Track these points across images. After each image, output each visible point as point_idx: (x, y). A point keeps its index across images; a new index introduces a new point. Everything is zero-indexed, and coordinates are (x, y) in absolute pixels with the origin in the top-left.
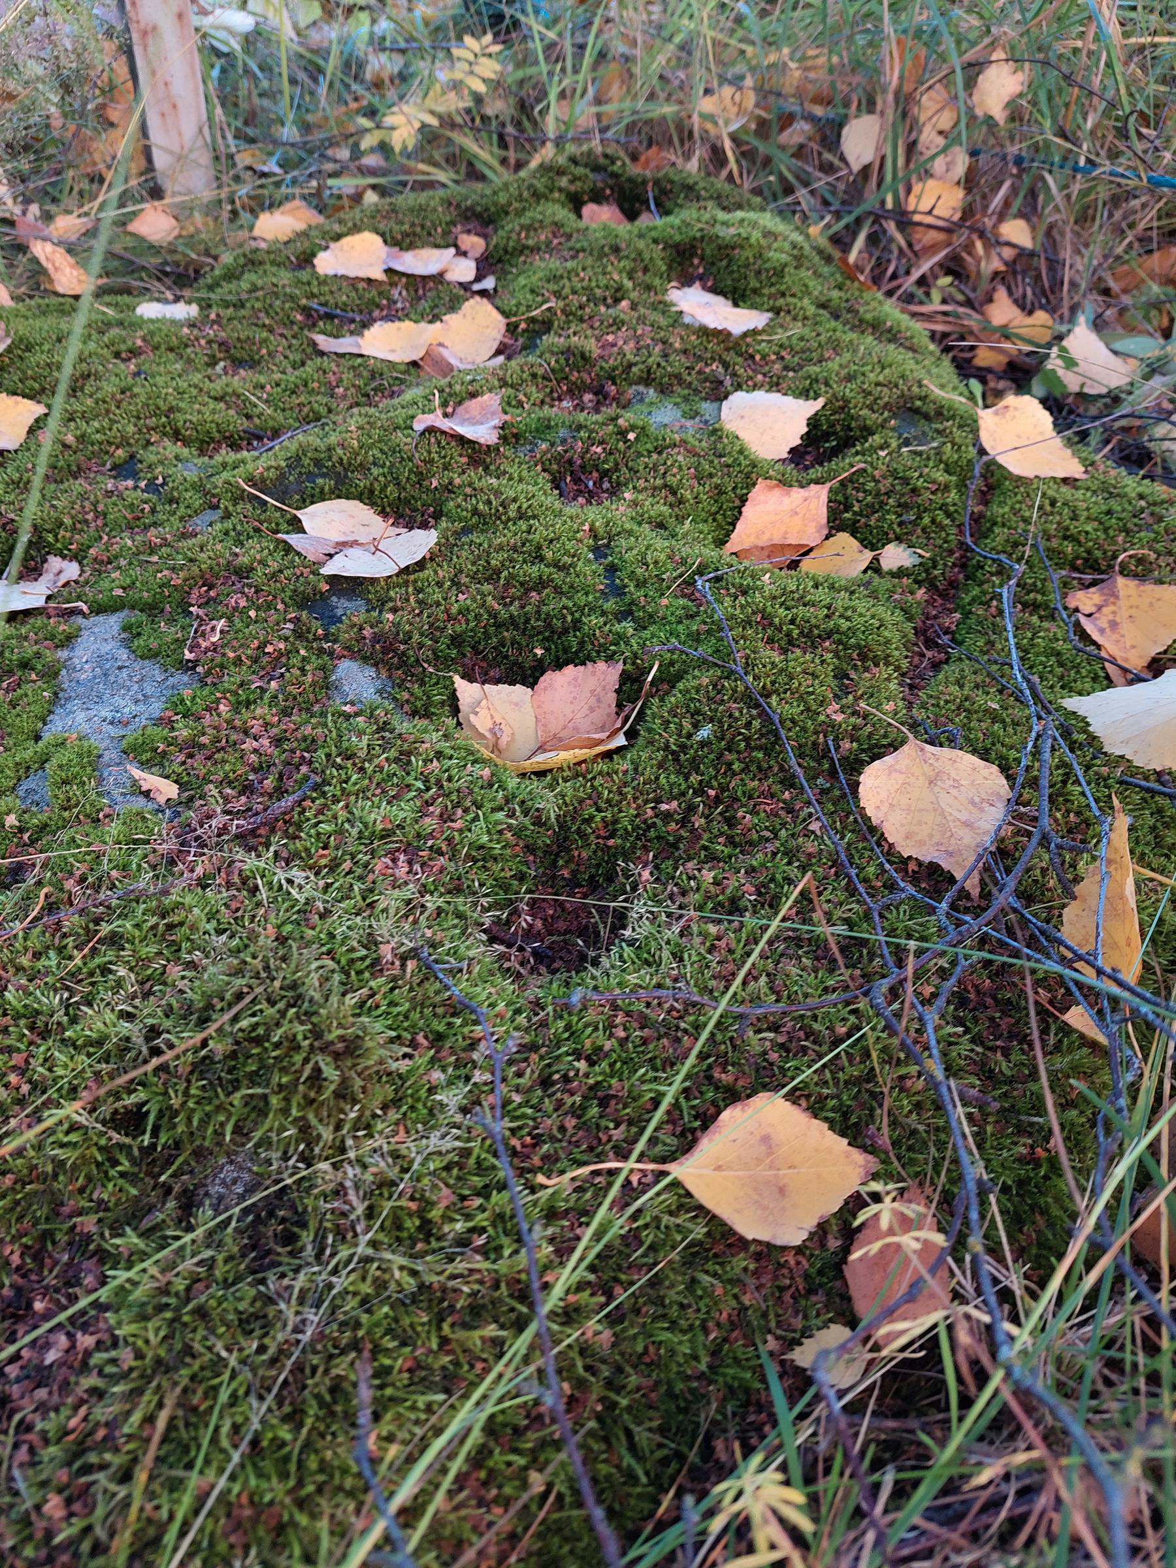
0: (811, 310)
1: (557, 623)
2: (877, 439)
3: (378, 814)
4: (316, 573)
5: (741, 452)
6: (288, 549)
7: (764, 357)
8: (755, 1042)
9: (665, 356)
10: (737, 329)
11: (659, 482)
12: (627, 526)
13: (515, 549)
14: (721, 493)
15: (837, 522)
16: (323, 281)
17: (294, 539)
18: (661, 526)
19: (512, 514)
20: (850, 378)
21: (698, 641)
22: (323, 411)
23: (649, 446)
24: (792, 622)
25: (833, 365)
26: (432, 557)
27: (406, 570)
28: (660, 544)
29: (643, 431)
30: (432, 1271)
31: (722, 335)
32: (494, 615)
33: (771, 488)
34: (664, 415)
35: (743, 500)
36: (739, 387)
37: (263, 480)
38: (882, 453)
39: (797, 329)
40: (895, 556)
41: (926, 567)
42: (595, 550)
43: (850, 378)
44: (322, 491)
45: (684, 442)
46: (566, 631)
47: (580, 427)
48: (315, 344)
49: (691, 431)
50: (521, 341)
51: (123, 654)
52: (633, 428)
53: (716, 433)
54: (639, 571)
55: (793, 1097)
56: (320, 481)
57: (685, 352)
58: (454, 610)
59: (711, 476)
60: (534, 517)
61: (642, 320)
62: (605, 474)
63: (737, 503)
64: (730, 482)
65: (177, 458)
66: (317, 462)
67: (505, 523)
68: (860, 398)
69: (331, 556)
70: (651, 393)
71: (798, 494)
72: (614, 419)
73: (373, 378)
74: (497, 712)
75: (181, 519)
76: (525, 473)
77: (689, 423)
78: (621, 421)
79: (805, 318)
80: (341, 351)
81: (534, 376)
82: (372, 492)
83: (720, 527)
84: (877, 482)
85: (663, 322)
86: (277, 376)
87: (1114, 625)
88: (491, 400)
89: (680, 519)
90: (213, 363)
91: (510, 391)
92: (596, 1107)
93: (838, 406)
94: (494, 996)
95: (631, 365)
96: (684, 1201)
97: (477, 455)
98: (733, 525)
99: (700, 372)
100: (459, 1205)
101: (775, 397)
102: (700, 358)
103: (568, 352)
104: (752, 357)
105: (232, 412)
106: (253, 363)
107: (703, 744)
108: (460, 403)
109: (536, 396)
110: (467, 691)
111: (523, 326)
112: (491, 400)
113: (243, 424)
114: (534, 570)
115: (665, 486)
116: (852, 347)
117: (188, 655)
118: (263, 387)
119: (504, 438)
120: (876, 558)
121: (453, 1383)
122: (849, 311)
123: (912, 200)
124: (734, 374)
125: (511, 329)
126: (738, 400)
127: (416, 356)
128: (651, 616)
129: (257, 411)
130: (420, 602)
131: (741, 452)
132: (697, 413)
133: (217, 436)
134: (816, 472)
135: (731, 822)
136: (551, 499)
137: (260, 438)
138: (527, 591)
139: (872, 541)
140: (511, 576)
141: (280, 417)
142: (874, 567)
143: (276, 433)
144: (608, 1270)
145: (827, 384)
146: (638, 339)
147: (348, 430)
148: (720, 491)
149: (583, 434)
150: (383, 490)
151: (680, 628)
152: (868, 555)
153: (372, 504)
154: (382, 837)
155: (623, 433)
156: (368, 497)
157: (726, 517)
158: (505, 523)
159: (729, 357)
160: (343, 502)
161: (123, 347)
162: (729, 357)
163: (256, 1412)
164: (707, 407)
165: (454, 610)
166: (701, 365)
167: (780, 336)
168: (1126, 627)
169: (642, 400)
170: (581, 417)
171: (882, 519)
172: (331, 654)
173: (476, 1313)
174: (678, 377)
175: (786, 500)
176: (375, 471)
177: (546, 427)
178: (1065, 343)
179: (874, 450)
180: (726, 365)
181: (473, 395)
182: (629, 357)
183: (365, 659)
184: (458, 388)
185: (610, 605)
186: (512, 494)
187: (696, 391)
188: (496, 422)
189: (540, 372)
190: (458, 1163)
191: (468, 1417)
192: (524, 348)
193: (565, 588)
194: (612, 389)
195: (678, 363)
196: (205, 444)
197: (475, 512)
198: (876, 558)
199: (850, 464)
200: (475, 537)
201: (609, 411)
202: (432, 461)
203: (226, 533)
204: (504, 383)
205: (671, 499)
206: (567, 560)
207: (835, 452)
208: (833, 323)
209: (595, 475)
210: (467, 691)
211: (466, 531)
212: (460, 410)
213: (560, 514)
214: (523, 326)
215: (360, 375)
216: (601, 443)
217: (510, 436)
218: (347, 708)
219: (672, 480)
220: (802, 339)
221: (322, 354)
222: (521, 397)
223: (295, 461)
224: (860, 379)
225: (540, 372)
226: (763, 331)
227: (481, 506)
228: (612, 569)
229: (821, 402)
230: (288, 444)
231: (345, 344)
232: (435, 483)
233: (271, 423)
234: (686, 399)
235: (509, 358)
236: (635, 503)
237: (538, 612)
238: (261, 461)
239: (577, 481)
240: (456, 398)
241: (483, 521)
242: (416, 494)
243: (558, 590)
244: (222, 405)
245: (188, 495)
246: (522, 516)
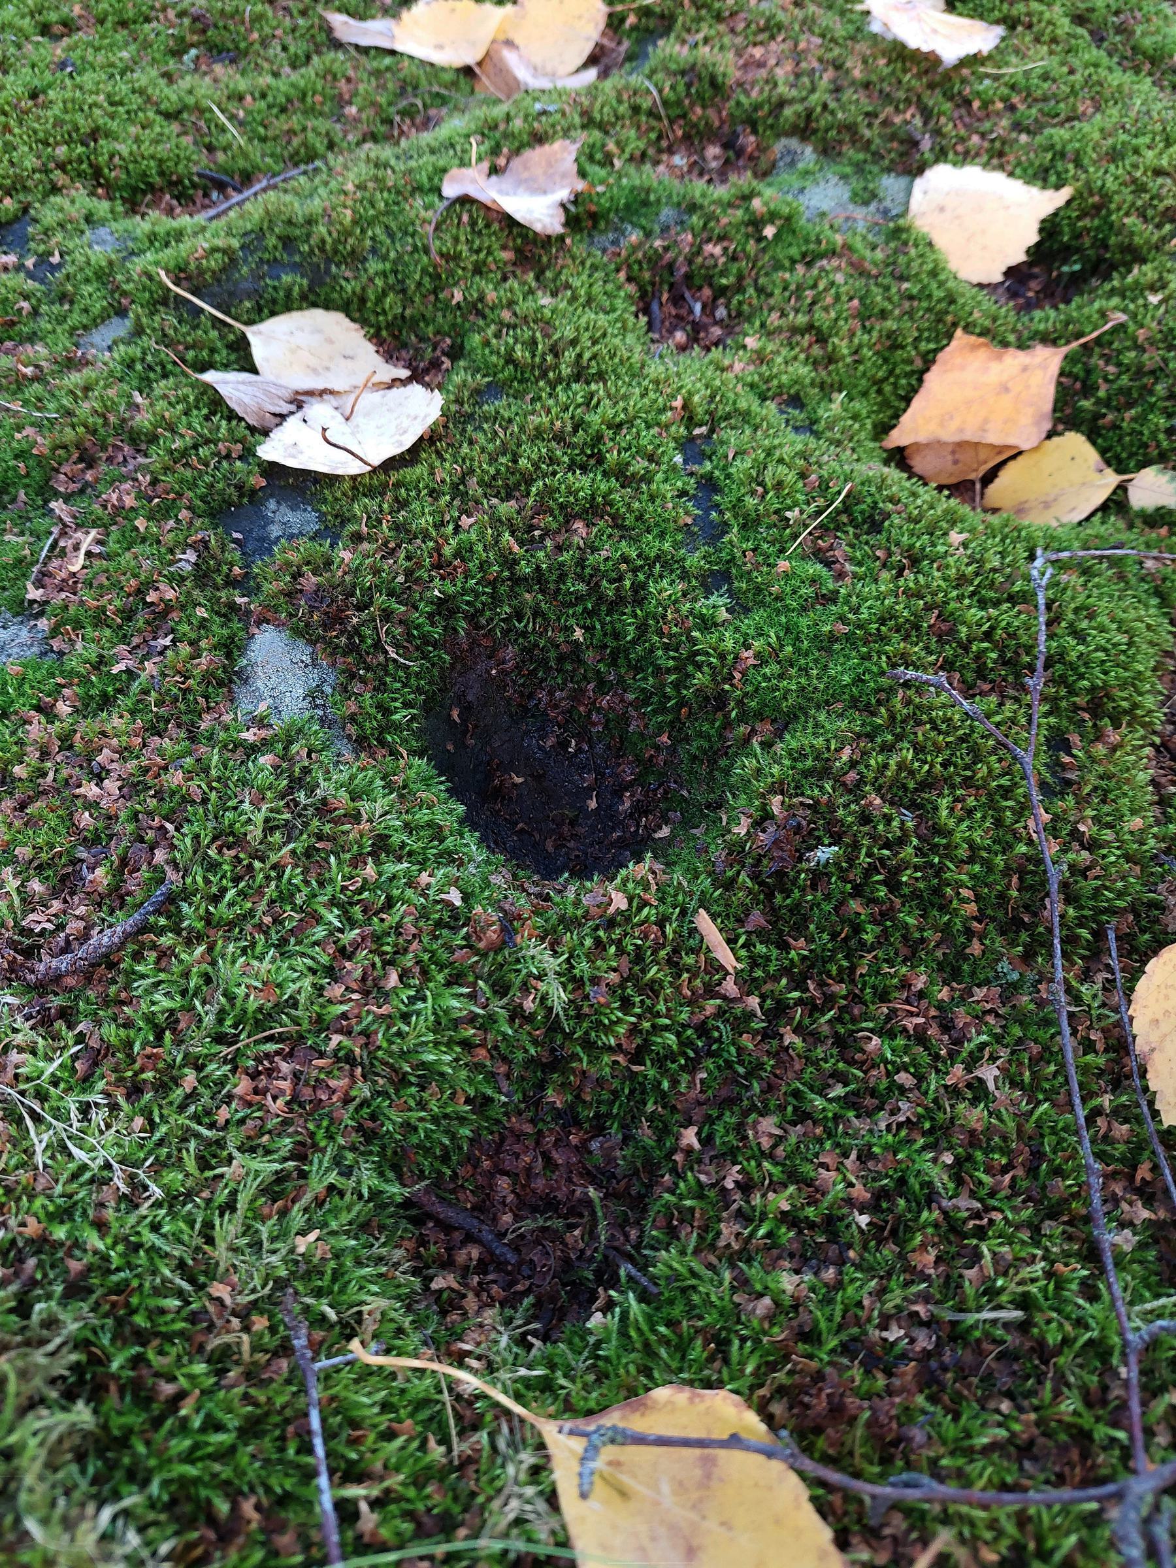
0: (1065, 25)
1: (608, 589)
2: (1144, 273)
4: (248, 454)
5: (934, 274)
6: (216, 403)
7: (986, 104)
9: (837, 90)
10: (950, 54)
11: (802, 319)
12: (743, 404)
13: (559, 438)
14: (896, 346)
15: (1067, 414)
17: (227, 383)
18: (796, 401)
19: (566, 371)
20: (1114, 156)
21: (829, 650)
22: (320, 146)
23: (794, 251)
24: (988, 635)
25: (1091, 128)
26: (428, 441)
27: (390, 465)
28: (792, 443)
29: (788, 223)
31: (929, 62)
32: (509, 562)
33: (974, 348)
34: (821, 196)
35: (929, 361)
36: (941, 155)
37: (201, 272)
38: (1154, 299)
39: (1040, 60)
42: (687, 445)
43: (1114, 156)
44: (289, 294)
45: (847, 247)
46: (620, 600)
47: (693, 207)
48: (329, 30)
49: (861, 227)
50: (626, 44)
52: (772, 217)
53: (898, 233)
54: (751, 501)
56: (287, 279)
57: (867, 85)
58: (447, 551)
59: (883, 315)
60: (601, 376)
61: (808, 24)
62: (722, 292)
63: (919, 364)
64: (915, 322)
65: (88, 219)
66: (287, 242)
67: (553, 385)
68: (1127, 195)
69: (282, 417)
70: (808, 154)
71: (1014, 359)
72: (747, 198)
73: (402, 92)
75: (72, 331)
76: (597, 288)
77: (860, 213)
78: (756, 203)
79: (1054, 40)
80: (364, 42)
81: (636, 109)
82: (363, 300)
83: (885, 404)
84: (1141, 349)
85: (840, 30)
86: (266, 80)
88: (563, 153)
89: (827, 390)
90: (177, 53)
91: (597, 134)
93: (1092, 205)
95: (782, 103)
97: (529, 249)
98: (908, 400)
99: (886, 123)
101: (998, 179)
102: (887, 98)
103: (689, 72)
104: (968, 103)
105: (186, 141)
106: (233, 54)
107: (819, 876)
108: (517, 152)
109: (636, 144)
111: (632, 19)
112: (563, 153)
113: (201, 162)
114: (582, 482)
115: (810, 327)
116: (1120, 97)
117: (34, 594)
118: (241, 98)
119: (573, 222)
120: (1122, 488)
122: (1119, 30)
124: (938, 132)
125: (614, 23)
126: (941, 180)
127: (470, 58)
128: (758, 590)
129: (223, 140)
130: (397, 527)
131: (934, 274)
132: (874, 195)
133: (157, 180)
134: (1046, 317)
135: (845, 1044)
136: (628, 342)
137: (221, 186)
138: (569, 518)
139: (1122, 456)
140: (550, 491)
141: (255, 152)
142: (1116, 504)
143: (247, 179)
145: (1078, 164)
146: (798, 56)
147: (324, 196)
148: (893, 342)
149: (695, 220)
150: (380, 300)
151: (804, 622)
152: (1111, 479)
153: (363, 322)
154: (259, 1025)
155: (756, 223)
156: (354, 308)
157: (897, 387)
158: (553, 385)
159: (934, 100)
160: (318, 314)
161: (53, 17)
162: (934, 100)
164: (890, 184)
165: (447, 551)
166: (890, 109)
167: (1014, 69)
169: (792, 164)
170: (698, 186)
171: (1142, 419)
172: (244, 614)
174: (850, 128)
175: (995, 367)
176: (374, 266)
177: (639, 205)
179: (1139, 289)
180: (927, 114)
181: (539, 139)
182: (782, 89)
183: (297, 632)
184: (517, 124)
185: (694, 560)
186: (569, 333)
187: (877, 156)
188: (564, 194)
189: (646, 104)
192: (630, 57)
193: (630, 520)
194: (750, 141)
195: (854, 106)
196: (136, 194)
197: (510, 360)
198: (1122, 488)
199: (1101, 310)
200: (501, 405)
201: (743, 180)
202: (457, 257)
203: (130, 365)
204: (589, 122)
205: (816, 351)
206: (639, 466)
207: (1075, 285)
208: (1095, 54)
209: (707, 292)
211: (494, 389)
212: (516, 163)
213: (637, 374)
214: (632, 19)
215: (382, 87)
216: (721, 238)
217: (582, 217)
218: (249, 736)
219: (822, 318)
220: (1045, 77)
221: (338, 45)
222: (611, 147)
223: (254, 239)
224: (1131, 159)
225: (646, 104)
226: (990, 57)
227: (519, 352)
228: (709, 485)
229: (1066, 193)
230: (252, 207)
231: (372, 32)
232: (458, 296)
233: (241, 163)
234: (859, 168)
235: (604, 74)
236: (760, 358)
237: (581, 563)
238: (205, 233)
239: (678, 300)
240: (505, 146)
241: (518, 378)
242: (429, 312)
243: (617, 522)
244: (175, 127)
245: (87, 289)
246: (580, 374)
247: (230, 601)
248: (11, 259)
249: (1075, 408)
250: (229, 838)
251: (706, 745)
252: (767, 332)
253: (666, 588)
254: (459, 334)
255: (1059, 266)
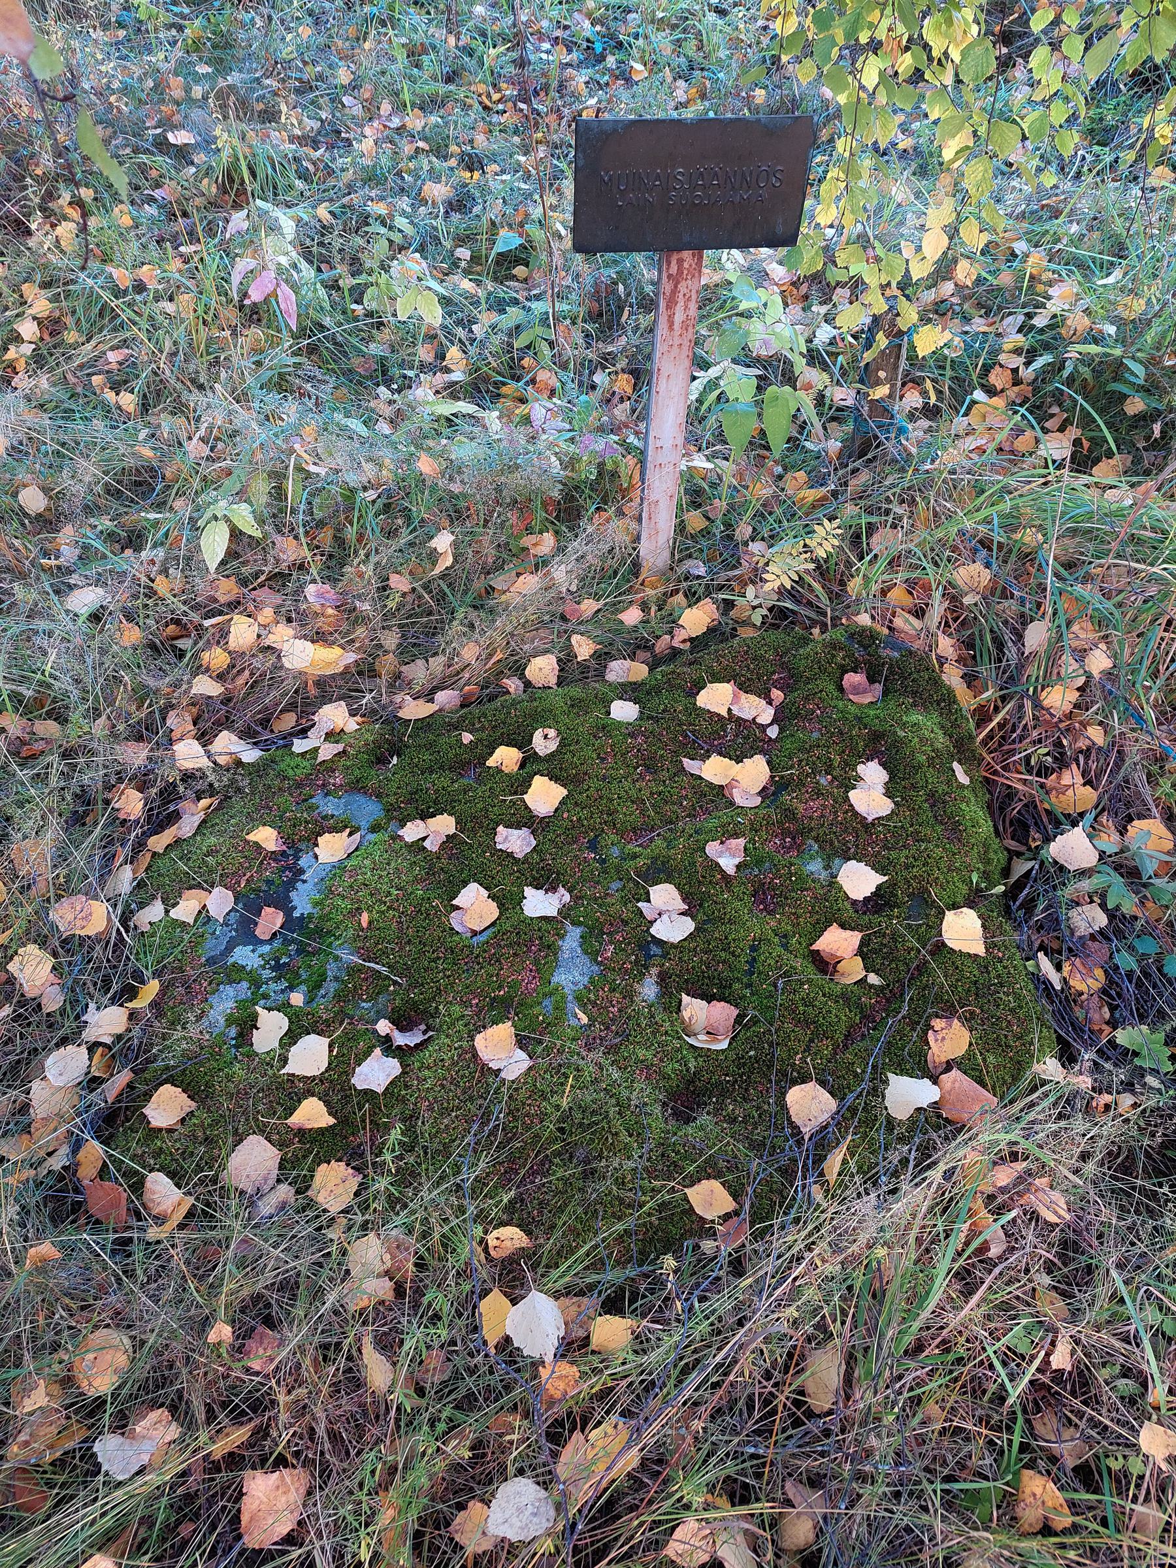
3: (641, 1053)
8: (722, 1164)
15: (860, 952)
16: (696, 708)
28: (780, 950)
30: (622, 1194)
40: (873, 979)
41: (882, 988)
51: (579, 950)
55: (723, 1184)
64: (832, 909)
71: (849, 933)
74: (694, 1009)
87: (943, 1039)
92: (673, 1165)
94: (657, 1120)
96: (686, 1199)
100: (632, 1181)
110: (686, 999)
114: (723, 954)
121: (620, 1219)
123: (1044, 694)
135: (746, 1090)
142: (863, 980)
144: (662, 1206)
163: (580, 1210)
168: (946, 1042)
173: (629, 1206)
178: (593, 1346)
190: (635, 1169)
191: (620, 1227)
210: (686, 999)
228: (754, 959)
247: (642, 969)
248: (1168, 1561)
249: (863, 951)
250: (639, 1025)
251: (994, 1251)
252: (783, 914)
253: (737, 986)
254: (702, 900)
255: (878, 901)
